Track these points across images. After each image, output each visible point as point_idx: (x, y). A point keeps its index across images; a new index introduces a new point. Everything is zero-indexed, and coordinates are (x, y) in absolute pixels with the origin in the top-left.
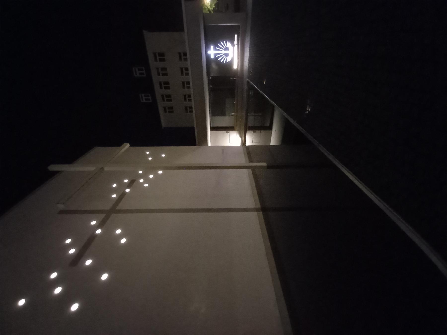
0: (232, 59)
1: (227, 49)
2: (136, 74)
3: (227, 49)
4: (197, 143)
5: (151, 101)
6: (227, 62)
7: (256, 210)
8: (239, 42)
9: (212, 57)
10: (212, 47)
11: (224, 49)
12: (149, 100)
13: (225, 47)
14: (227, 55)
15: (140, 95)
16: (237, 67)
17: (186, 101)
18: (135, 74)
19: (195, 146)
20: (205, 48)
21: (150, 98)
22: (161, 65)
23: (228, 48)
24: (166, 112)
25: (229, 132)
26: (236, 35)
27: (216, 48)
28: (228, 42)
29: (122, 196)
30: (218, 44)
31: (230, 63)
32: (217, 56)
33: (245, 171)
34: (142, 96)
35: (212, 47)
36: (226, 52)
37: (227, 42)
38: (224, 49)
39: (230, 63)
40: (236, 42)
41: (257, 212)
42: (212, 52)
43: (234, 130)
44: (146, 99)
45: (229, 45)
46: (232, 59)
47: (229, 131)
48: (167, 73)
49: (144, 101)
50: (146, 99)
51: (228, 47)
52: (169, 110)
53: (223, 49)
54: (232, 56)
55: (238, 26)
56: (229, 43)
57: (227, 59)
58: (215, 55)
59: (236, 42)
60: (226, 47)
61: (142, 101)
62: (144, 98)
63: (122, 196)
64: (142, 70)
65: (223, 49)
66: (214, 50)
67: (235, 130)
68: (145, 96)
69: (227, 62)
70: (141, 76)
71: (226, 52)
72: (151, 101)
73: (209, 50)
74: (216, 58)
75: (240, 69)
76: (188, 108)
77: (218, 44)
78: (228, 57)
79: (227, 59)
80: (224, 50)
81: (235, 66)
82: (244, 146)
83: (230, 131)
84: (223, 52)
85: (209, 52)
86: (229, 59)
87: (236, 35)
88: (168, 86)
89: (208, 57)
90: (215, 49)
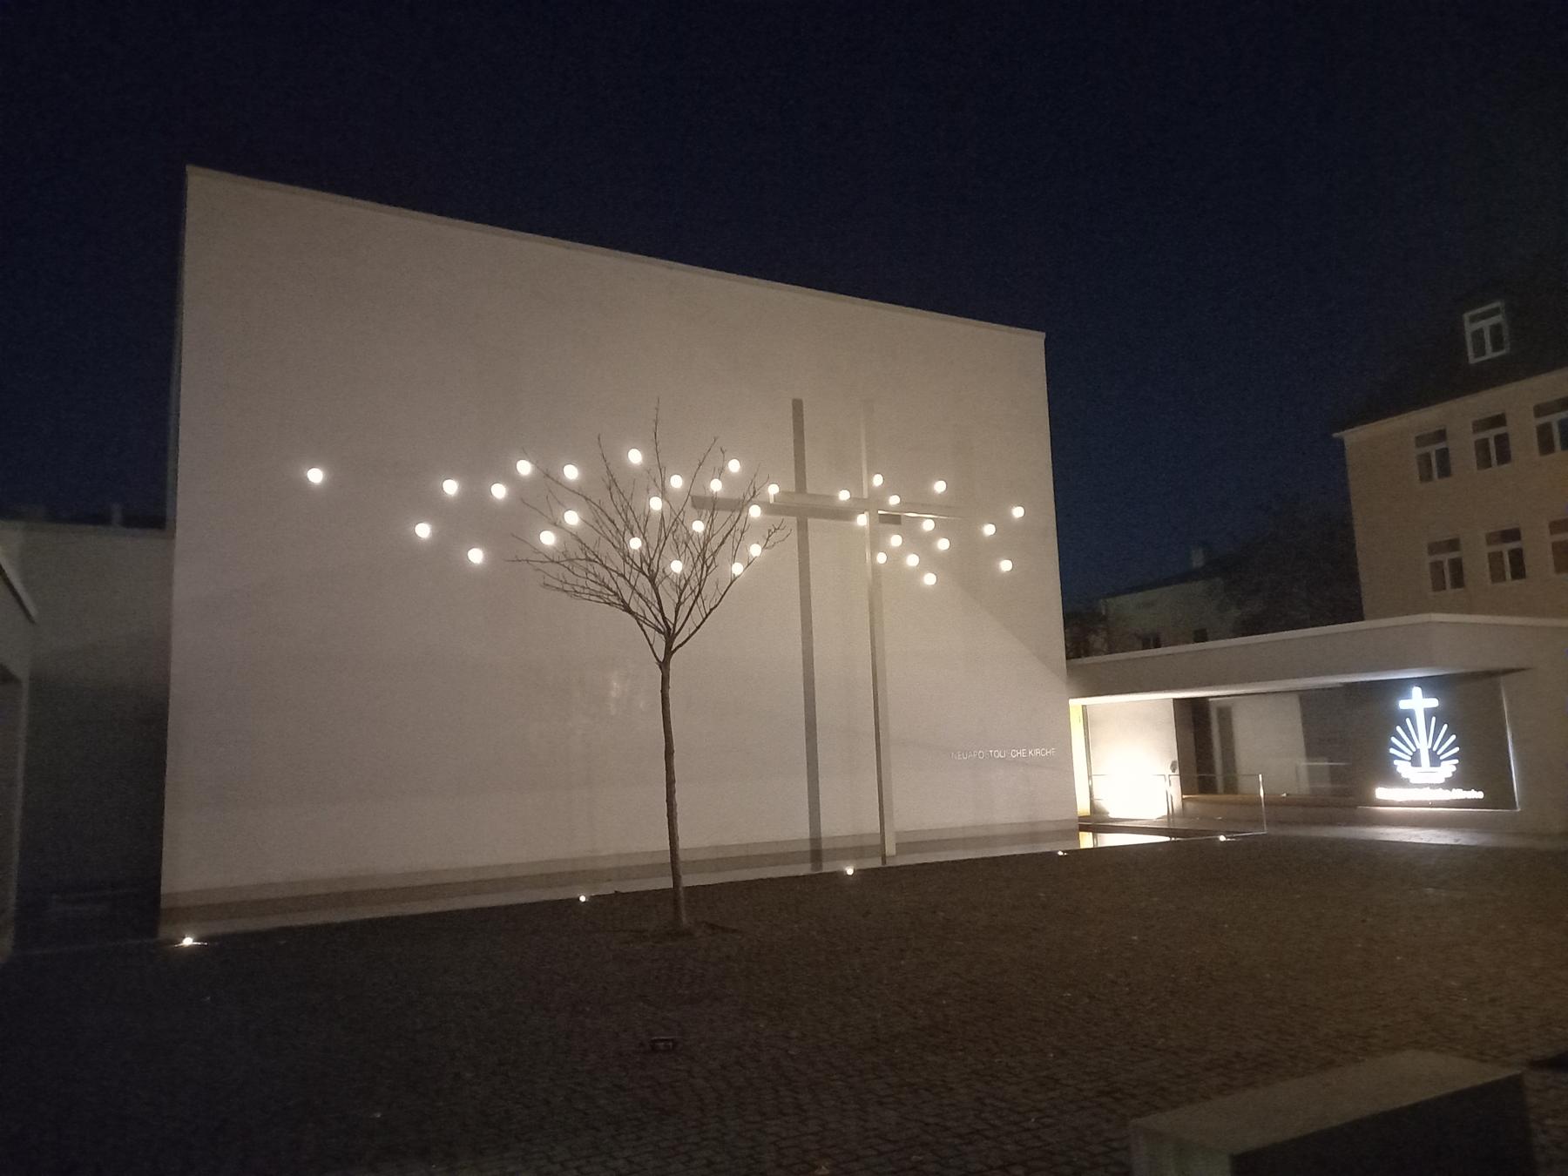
0: (1404, 783)
1: (1435, 760)
2: (1473, 319)
3: (1435, 760)
4: (1079, 661)
6: (1396, 762)
7: (816, 840)
8: (1304, 805)
9: (1403, 704)
10: (1434, 703)
11: (1435, 749)
12: (1480, 350)
14: (1415, 760)
17: (1489, 543)
19: (1062, 653)
21: (1490, 354)
22: (1523, 431)
23: (1439, 765)
24: (1422, 440)
25: (1174, 771)
26: (1480, 795)
27: (1434, 719)
28: (1456, 765)
29: (845, 514)
31: (1392, 778)
32: (1408, 720)
34: (1495, 312)
35: (1434, 703)
36: (1425, 758)
37: (1456, 761)
38: (1435, 749)
39: (1392, 778)
40: (1459, 794)
41: (811, 839)
42: (1418, 702)
43: (1183, 794)
45: (1448, 768)
46: (1404, 783)
47: (1177, 772)
49: (1470, 329)
50: (1478, 335)
51: (1443, 763)
53: (1433, 746)
55: (1510, 804)
56: (1454, 769)
57: (1403, 760)
58: (1410, 714)
59: (1459, 794)
60: (1442, 758)
61: (1466, 316)
62: (1485, 324)
63: (845, 514)
64: (1497, 345)
65: (1433, 746)
66: (1425, 709)
67: (1184, 797)
68: (1496, 329)
70: (1469, 340)
72: (1473, 360)
74: (1403, 717)
75: (1379, 812)
76: (1513, 545)
77: (1445, 726)
78: (1410, 763)
79: (1403, 760)
81: (1381, 793)
82: (1075, 826)
83: (1178, 777)
84: (1423, 745)
85: (1417, 691)
86: (1403, 768)
87: (1480, 795)
89: (1401, 687)
90: (1429, 713)
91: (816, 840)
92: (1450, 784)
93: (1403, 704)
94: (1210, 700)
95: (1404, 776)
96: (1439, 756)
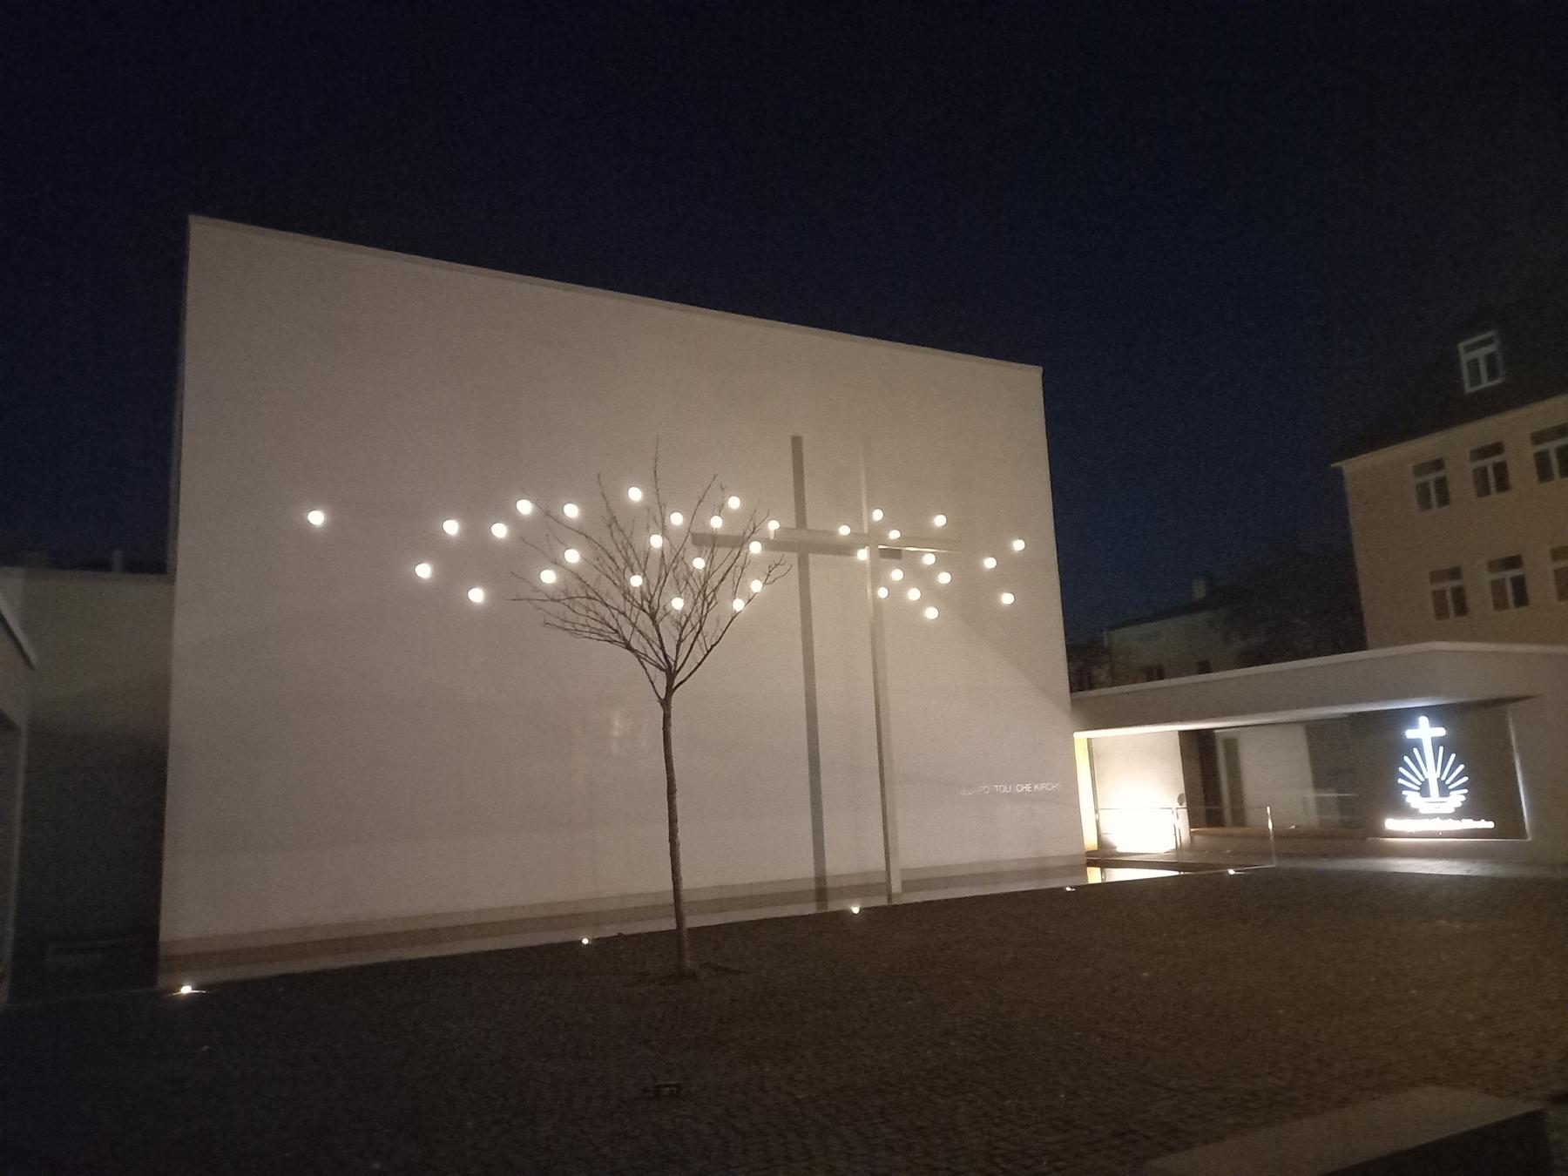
1: (1444, 790)
2: (1469, 349)
3: (1444, 790)
5: (1469, 389)
6: (1404, 793)
7: (820, 878)
9: (1410, 734)
11: (1443, 778)
12: (1476, 379)
13: (1448, 782)
14: (1424, 790)
15: (1488, 335)
16: (1397, 832)
18: (1469, 342)
20: (1441, 705)
21: (1486, 383)
23: (1448, 795)
25: (1181, 804)
26: (1491, 825)
27: (1441, 748)
30: (1453, 756)
31: (1402, 810)
32: (1415, 750)
33: (882, 865)
34: (1489, 341)
35: (1441, 732)
36: (1434, 788)
37: (1466, 791)
38: (1443, 778)
39: (1402, 810)
44: (1474, 363)
45: (1457, 799)
47: (1185, 805)
48: (1487, 492)
49: (1465, 358)
51: (1451, 793)
52: (1490, 471)
54: (1421, 811)
55: (1520, 833)
56: (1464, 798)
58: (1417, 744)
61: (1461, 346)
62: (1481, 353)
64: (1492, 373)
65: (1441, 776)
67: (1192, 830)
68: (1490, 358)
69: (1404, 793)
71: (1434, 788)
72: (1469, 389)
73: (1412, 728)
80: (1439, 779)
81: (1391, 824)
83: (1186, 810)
84: (1432, 774)
85: (1423, 720)
86: (1412, 798)
87: (1491, 825)
88: (1493, 489)
89: (1408, 717)
90: (1437, 743)
91: (820, 878)
92: (1460, 814)
93: (1410, 734)
94: (1216, 731)
95: (1413, 806)
96: (1445, 781)
